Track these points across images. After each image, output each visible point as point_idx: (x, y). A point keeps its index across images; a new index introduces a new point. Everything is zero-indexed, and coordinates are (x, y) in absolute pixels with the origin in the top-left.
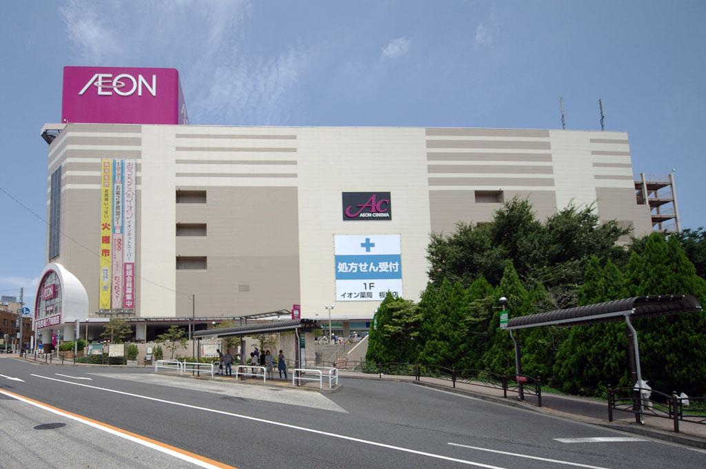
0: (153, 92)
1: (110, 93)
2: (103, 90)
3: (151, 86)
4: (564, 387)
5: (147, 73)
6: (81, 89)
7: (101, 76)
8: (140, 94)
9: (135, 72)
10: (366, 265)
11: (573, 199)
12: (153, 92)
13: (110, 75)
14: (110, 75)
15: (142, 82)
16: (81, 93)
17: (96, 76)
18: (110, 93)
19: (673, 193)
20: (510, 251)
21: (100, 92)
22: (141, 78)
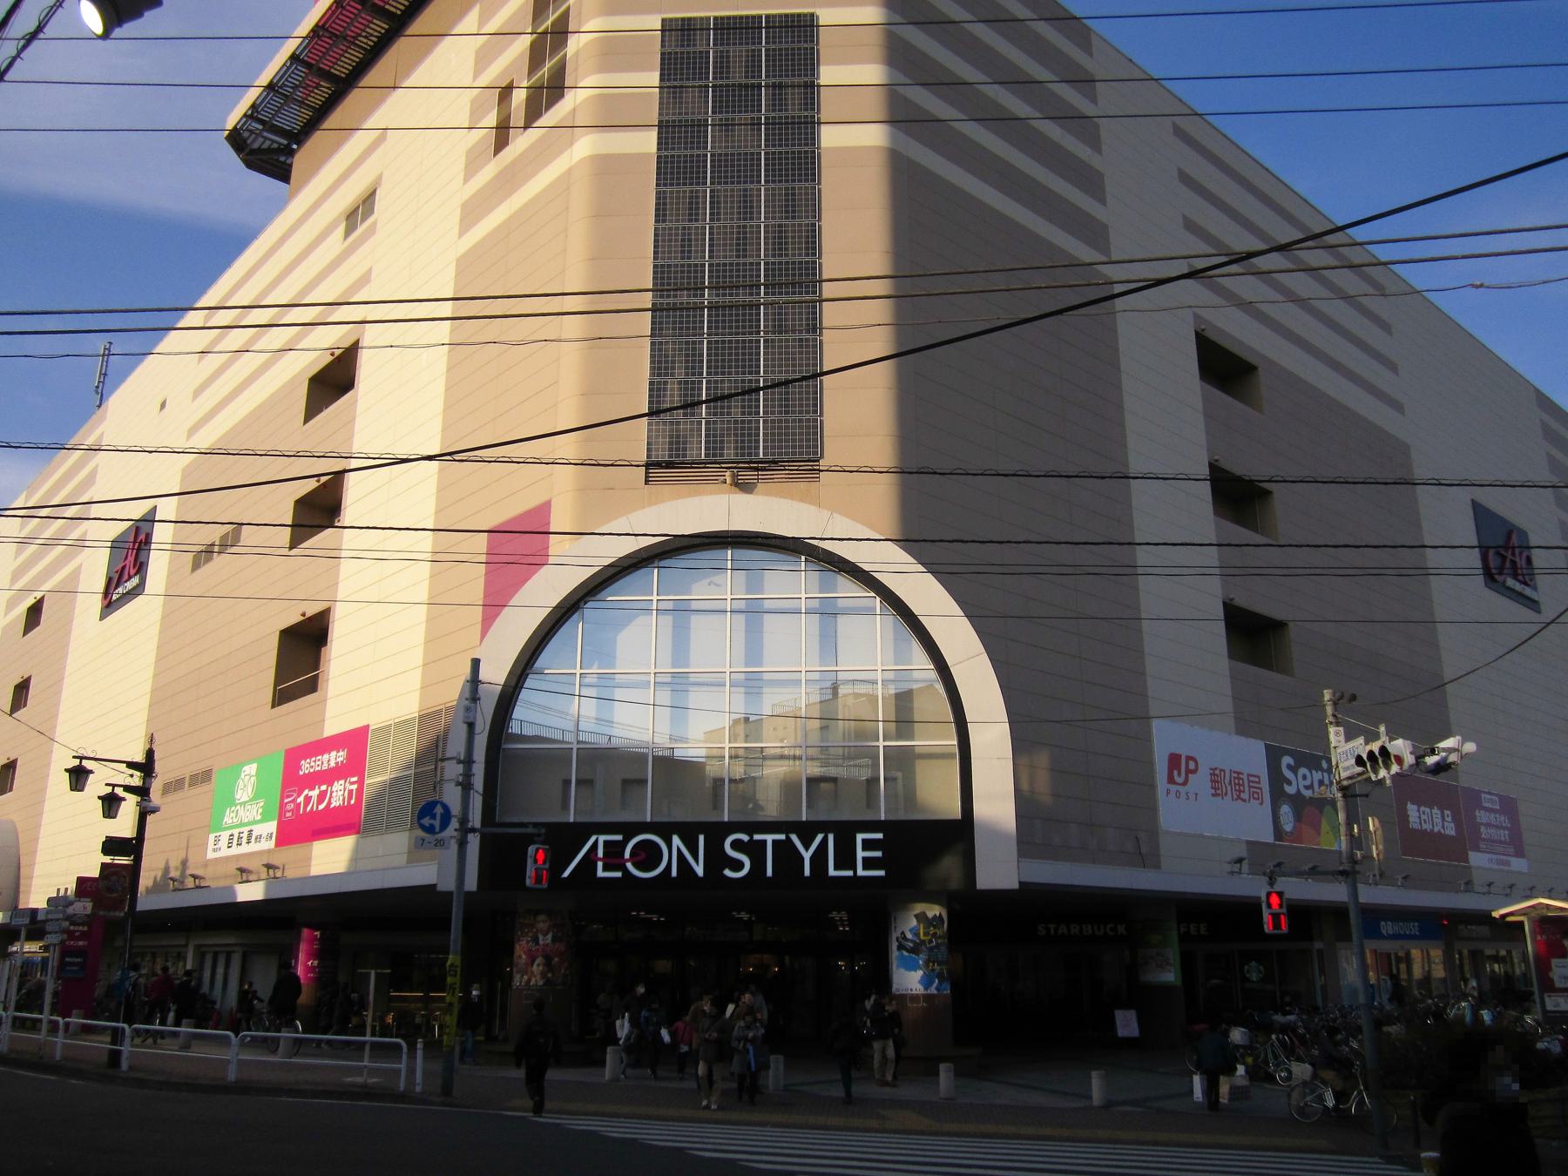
0: (700, 870)
1: (618, 874)
2: (605, 869)
3: (696, 859)
4: (422, 821)
5: (689, 833)
6: (565, 870)
7: (602, 838)
8: (674, 873)
9: (665, 830)
10: (1060, 932)
11: (1232, 873)
12: (700, 870)
13: (619, 837)
14: (619, 837)
15: (698, 864)
16: (566, 874)
17: (593, 839)
18: (618, 874)
19: (938, 274)
20: (1419, 996)
21: (601, 873)
22: (676, 840)
